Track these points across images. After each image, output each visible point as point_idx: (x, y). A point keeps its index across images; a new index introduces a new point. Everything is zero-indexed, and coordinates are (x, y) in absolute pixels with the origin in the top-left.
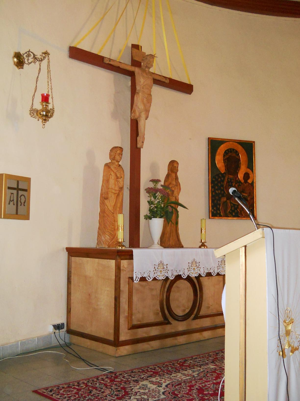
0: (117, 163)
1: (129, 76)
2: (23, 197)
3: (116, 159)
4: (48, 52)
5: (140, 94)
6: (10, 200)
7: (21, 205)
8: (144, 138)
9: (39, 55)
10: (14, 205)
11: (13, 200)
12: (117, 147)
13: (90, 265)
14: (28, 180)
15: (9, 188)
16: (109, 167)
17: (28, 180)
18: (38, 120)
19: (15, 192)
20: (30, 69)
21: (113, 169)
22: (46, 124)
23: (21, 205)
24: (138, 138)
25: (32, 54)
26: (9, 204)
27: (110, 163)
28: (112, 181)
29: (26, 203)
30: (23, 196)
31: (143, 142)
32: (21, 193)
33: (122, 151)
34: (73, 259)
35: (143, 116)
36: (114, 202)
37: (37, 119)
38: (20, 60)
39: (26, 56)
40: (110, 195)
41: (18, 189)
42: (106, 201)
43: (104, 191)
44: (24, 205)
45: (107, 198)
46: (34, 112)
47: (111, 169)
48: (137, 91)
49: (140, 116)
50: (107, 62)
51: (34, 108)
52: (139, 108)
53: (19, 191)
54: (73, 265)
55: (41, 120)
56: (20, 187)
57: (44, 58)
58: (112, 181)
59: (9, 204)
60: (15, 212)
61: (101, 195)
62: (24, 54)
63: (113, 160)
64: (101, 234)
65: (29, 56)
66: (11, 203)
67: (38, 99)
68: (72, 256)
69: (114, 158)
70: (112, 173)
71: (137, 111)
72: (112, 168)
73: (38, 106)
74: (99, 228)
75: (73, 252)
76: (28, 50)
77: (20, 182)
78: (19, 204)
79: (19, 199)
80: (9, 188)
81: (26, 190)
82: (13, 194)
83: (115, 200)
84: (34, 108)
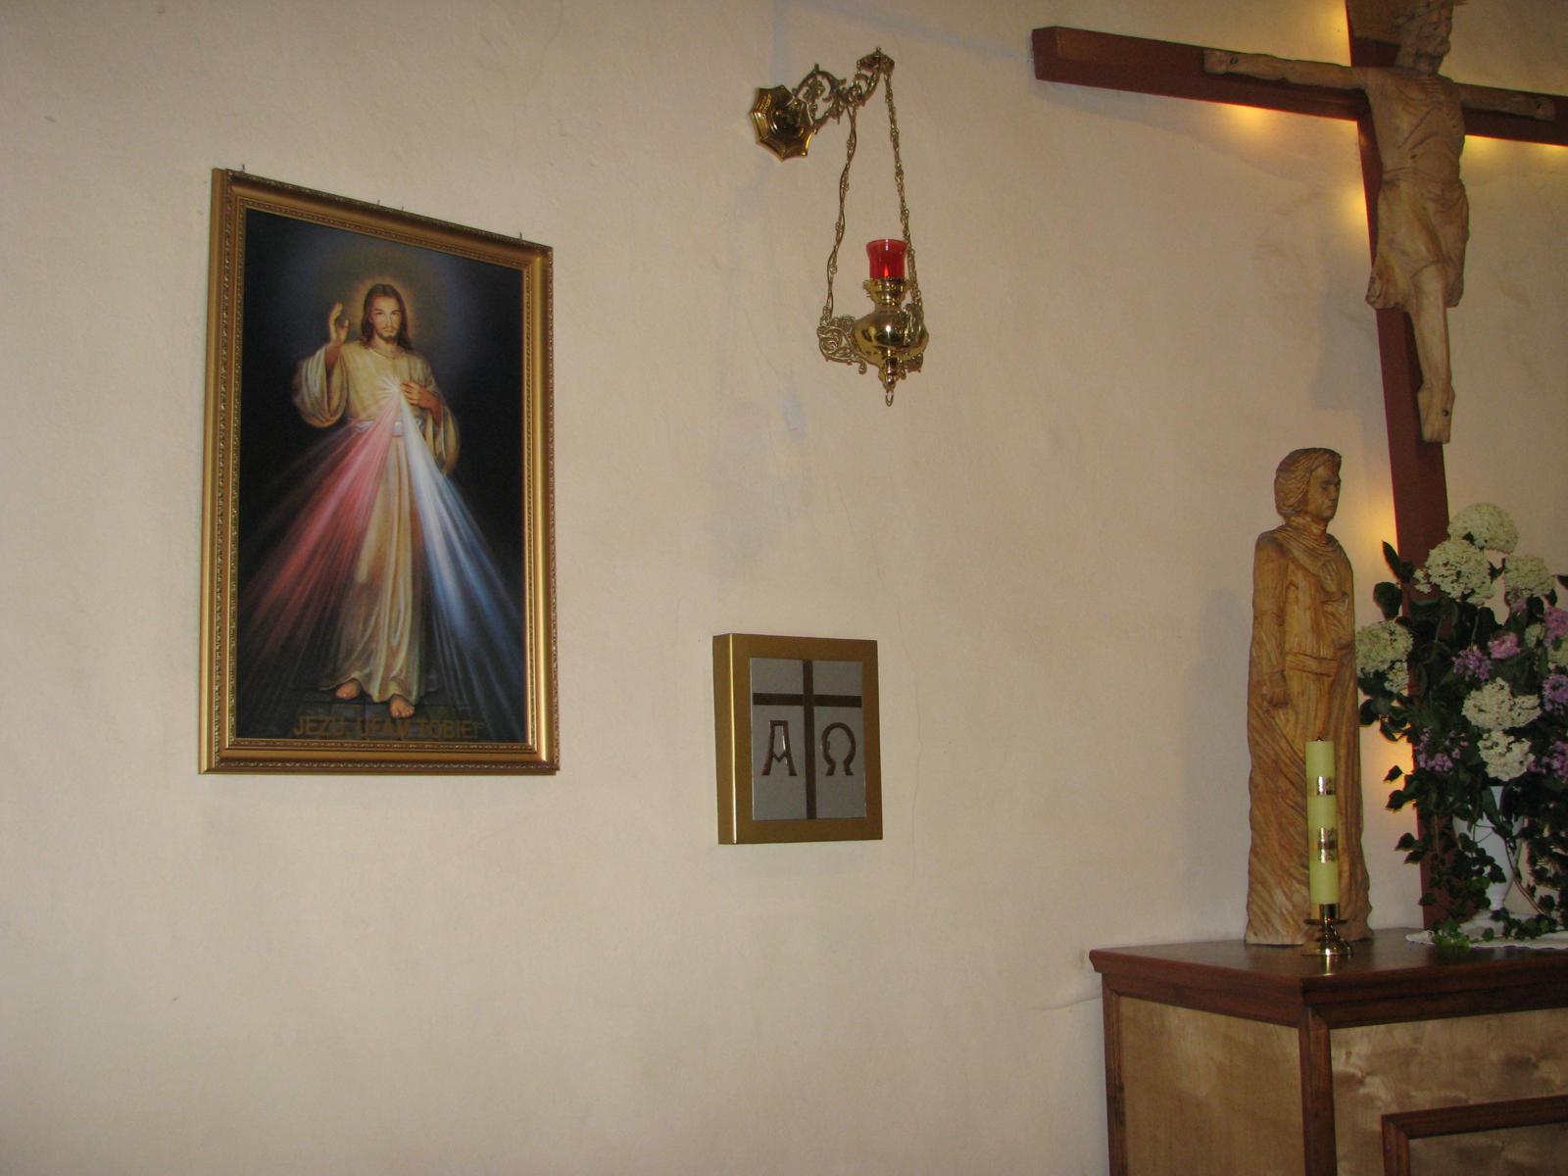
0: (1316, 529)
1: (1353, 119)
2: (838, 738)
3: (1311, 508)
4: (884, 51)
5: (1403, 185)
6: (772, 755)
7: (831, 773)
8: (1449, 394)
9: (846, 71)
10: (792, 773)
11: (787, 754)
12: (1314, 450)
13: (1194, 1038)
14: (863, 653)
15: (761, 699)
16: (1282, 550)
17: (863, 653)
18: (863, 371)
19: (794, 715)
20: (825, 142)
21: (1304, 559)
22: (900, 383)
23: (831, 773)
24: (1423, 398)
25: (825, 83)
26: (766, 772)
27: (1281, 529)
28: (1300, 618)
29: (865, 756)
30: (836, 733)
31: (1447, 413)
32: (824, 716)
33: (1338, 465)
34: (1128, 1005)
35: (1433, 285)
36: (1321, 714)
37: (856, 365)
38: (785, 125)
39: (806, 96)
40: (1295, 686)
41: (808, 700)
42: (1280, 717)
43: (1266, 669)
44: (848, 772)
45: (1282, 702)
46: (840, 338)
47: (1295, 560)
48: (1386, 177)
49: (1417, 290)
50: (1221, 69)
51: (836, 314)
52: (1403, 252)
53: (817, 709)
54: (1129, 1036)
55: (873, 370)
56: (820, 688)
57: (872, 82)
58: (1300, 618)
59: (766, 772)
60: (801, 811)
61: (1254, 687)
62: (797, 91)
63: (1298, 513)
64: (1271, 880)
65: (813, 95)
66: (780, 768)
67: (857, 267)
68: (1120, 994)
69: (1304, 500)
70: (1299, 578)
71: (1397, 270)
72: (1296, 553)
73: (857, 304)
74: (1254, 851)
75: (1130, 979)
76: (810, 69)
77: (816, 664)
78: (821, 766)
79: (819, 747)
80: (761, 699)
81: (853, 702)
82: (784, 724)
83: (1322, 707)
84: (836, 314)
